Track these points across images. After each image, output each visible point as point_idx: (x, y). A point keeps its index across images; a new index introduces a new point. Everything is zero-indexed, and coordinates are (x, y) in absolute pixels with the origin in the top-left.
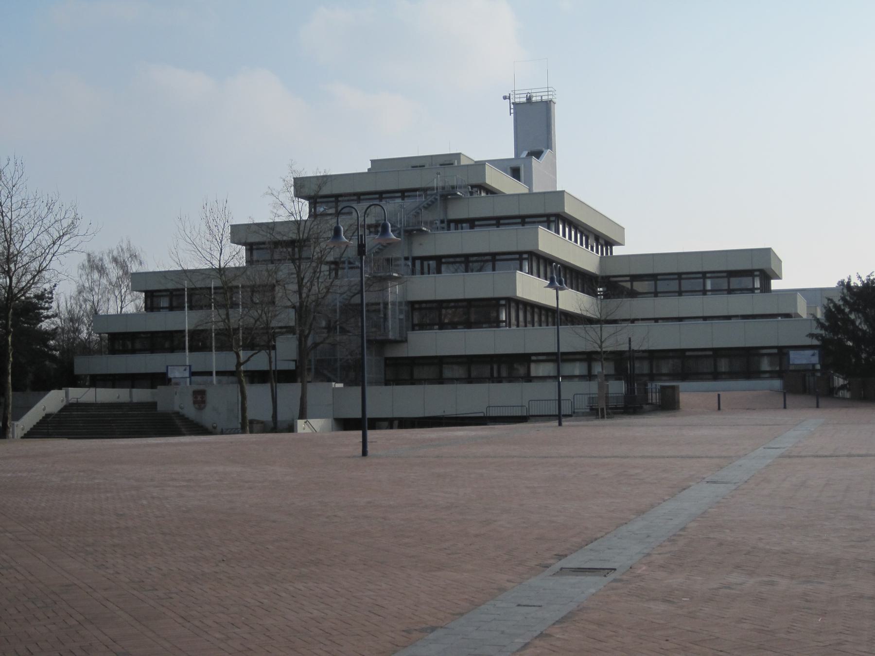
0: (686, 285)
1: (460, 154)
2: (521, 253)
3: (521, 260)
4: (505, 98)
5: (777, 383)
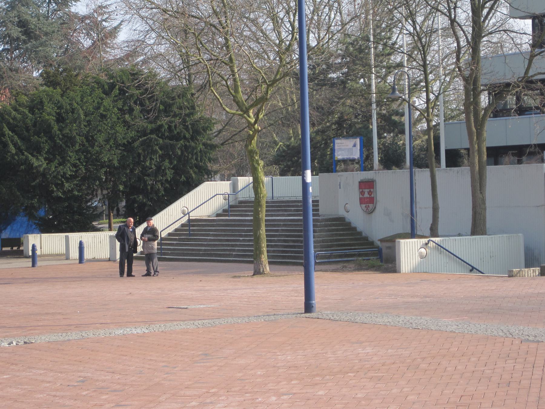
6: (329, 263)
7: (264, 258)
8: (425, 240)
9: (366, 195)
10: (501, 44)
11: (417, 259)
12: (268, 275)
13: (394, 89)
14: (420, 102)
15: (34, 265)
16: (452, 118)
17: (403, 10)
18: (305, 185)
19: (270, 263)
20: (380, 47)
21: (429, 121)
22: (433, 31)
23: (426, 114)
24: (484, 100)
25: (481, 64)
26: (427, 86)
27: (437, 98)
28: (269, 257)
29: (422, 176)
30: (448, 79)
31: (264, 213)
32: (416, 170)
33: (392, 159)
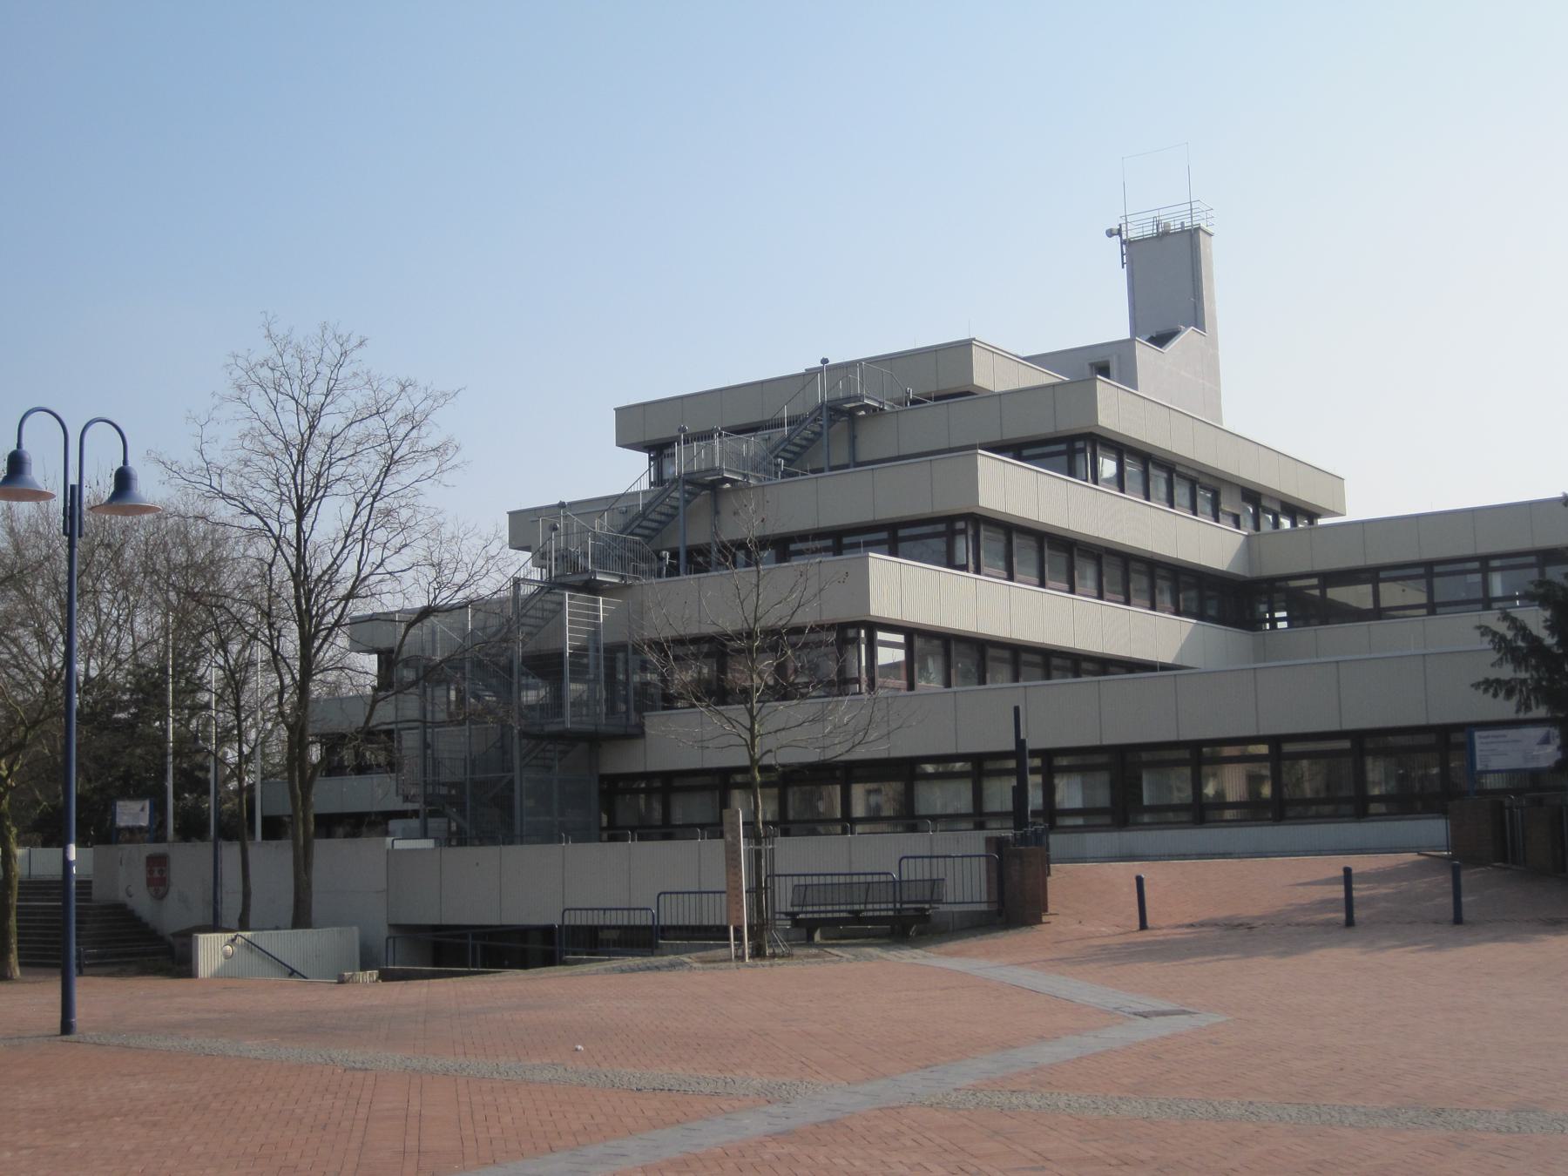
0: (1446, 588)
1: (965, 346)
2: (950, 520)
3: (950, 535)
4: (1110, 233)
5: (1434, 830)
6: (106, 964)
7: (13, 959)
8: (230, 936)
9: (156, 875)
10: (337, 686)
11: (221, 960)
12: (17, 981)
13: (196, 738)
14: (232, 755)
15: (911, 686)
16: (274, 775)
17: (212, 636)
18: (67, 864)
19: (21, 965)
20: (183, 683)
21: (241, 780)
22: (251, 663)
23: (238, 772)
24: (315, 754)
25: (310, 709)
26: (240, 735)
27: (253, 750)
28: (20, 956)
29: (230, 853)
30: (269, 725)
31: (15, 896)
32: (224, 844)
33: (191, 828)
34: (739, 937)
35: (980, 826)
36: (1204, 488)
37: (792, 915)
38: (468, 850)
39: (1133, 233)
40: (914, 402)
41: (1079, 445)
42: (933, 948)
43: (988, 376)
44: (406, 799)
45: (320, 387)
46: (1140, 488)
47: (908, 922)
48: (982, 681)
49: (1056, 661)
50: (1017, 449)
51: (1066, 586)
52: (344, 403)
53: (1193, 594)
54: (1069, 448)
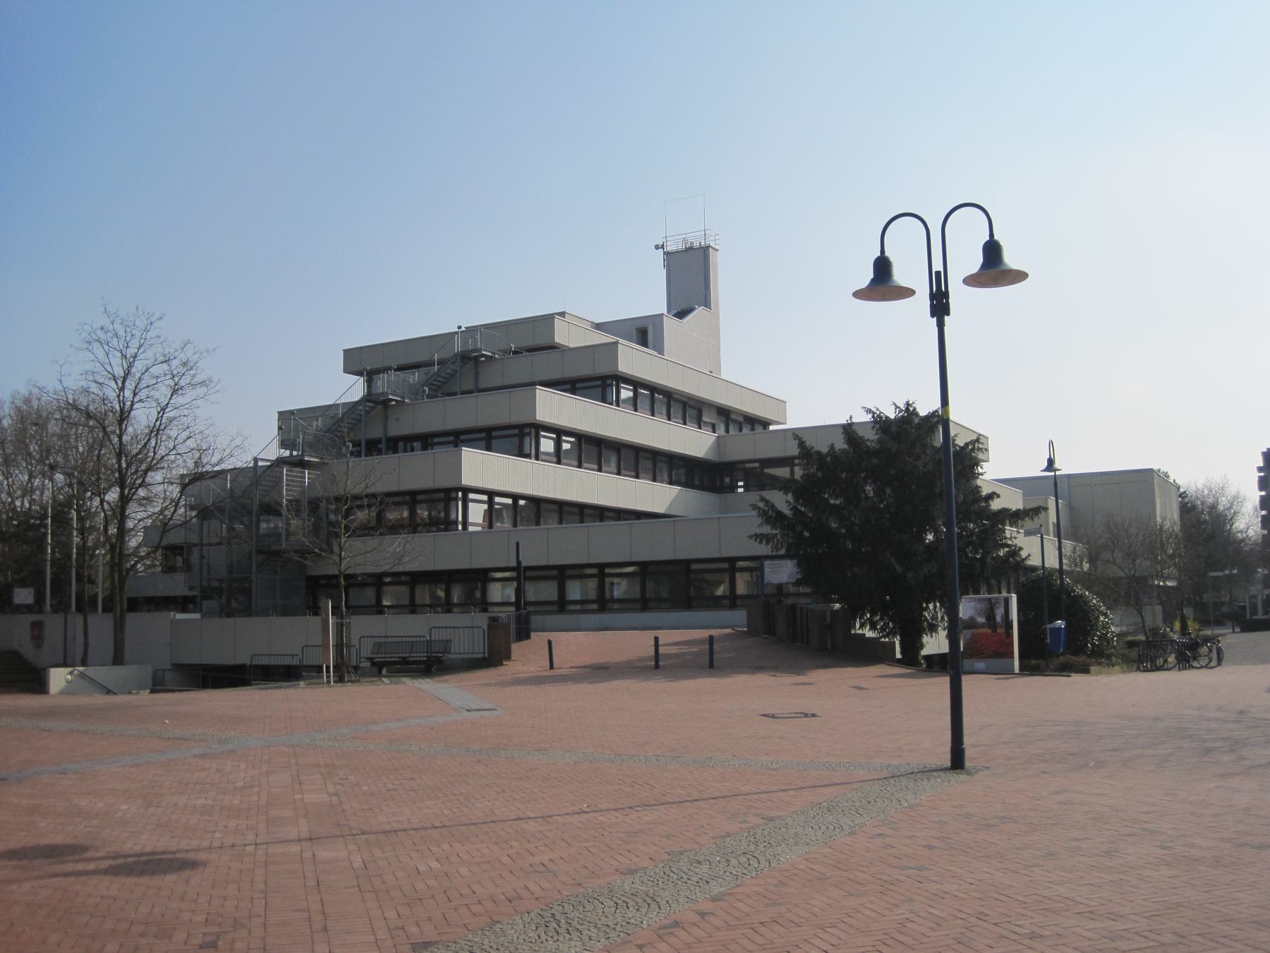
2: (521, 427)
3: (521, 436)
4: (657, 247)
8: (70, 669)
33: (61, 607)
34: (328, 671)
35: (485, 610)
36: (691, 407)
37: (370, 659)
38: (290, 619)
39: (670, 248)
40: (515, 353)
41: (609, 382)
42: (437, 679)
43: (564, 336)
44: (191, 589)
45: (134, 344)
46: (648, 407)
47: (432, 663)
48: (538, 523)
49: (587, 511)
50: (571, 385)
51: (596, 467)
52: (150, 354)
53: (682, 471)
54: (598, 383)
